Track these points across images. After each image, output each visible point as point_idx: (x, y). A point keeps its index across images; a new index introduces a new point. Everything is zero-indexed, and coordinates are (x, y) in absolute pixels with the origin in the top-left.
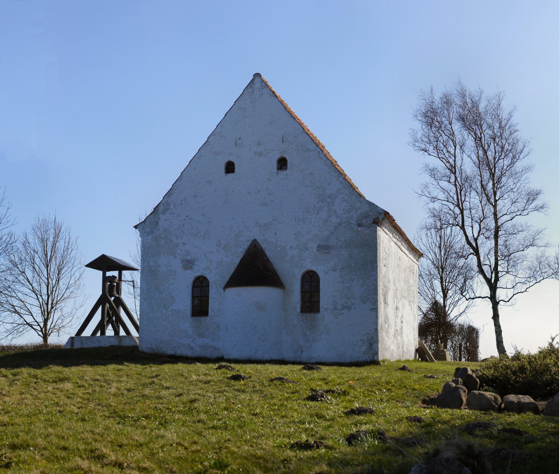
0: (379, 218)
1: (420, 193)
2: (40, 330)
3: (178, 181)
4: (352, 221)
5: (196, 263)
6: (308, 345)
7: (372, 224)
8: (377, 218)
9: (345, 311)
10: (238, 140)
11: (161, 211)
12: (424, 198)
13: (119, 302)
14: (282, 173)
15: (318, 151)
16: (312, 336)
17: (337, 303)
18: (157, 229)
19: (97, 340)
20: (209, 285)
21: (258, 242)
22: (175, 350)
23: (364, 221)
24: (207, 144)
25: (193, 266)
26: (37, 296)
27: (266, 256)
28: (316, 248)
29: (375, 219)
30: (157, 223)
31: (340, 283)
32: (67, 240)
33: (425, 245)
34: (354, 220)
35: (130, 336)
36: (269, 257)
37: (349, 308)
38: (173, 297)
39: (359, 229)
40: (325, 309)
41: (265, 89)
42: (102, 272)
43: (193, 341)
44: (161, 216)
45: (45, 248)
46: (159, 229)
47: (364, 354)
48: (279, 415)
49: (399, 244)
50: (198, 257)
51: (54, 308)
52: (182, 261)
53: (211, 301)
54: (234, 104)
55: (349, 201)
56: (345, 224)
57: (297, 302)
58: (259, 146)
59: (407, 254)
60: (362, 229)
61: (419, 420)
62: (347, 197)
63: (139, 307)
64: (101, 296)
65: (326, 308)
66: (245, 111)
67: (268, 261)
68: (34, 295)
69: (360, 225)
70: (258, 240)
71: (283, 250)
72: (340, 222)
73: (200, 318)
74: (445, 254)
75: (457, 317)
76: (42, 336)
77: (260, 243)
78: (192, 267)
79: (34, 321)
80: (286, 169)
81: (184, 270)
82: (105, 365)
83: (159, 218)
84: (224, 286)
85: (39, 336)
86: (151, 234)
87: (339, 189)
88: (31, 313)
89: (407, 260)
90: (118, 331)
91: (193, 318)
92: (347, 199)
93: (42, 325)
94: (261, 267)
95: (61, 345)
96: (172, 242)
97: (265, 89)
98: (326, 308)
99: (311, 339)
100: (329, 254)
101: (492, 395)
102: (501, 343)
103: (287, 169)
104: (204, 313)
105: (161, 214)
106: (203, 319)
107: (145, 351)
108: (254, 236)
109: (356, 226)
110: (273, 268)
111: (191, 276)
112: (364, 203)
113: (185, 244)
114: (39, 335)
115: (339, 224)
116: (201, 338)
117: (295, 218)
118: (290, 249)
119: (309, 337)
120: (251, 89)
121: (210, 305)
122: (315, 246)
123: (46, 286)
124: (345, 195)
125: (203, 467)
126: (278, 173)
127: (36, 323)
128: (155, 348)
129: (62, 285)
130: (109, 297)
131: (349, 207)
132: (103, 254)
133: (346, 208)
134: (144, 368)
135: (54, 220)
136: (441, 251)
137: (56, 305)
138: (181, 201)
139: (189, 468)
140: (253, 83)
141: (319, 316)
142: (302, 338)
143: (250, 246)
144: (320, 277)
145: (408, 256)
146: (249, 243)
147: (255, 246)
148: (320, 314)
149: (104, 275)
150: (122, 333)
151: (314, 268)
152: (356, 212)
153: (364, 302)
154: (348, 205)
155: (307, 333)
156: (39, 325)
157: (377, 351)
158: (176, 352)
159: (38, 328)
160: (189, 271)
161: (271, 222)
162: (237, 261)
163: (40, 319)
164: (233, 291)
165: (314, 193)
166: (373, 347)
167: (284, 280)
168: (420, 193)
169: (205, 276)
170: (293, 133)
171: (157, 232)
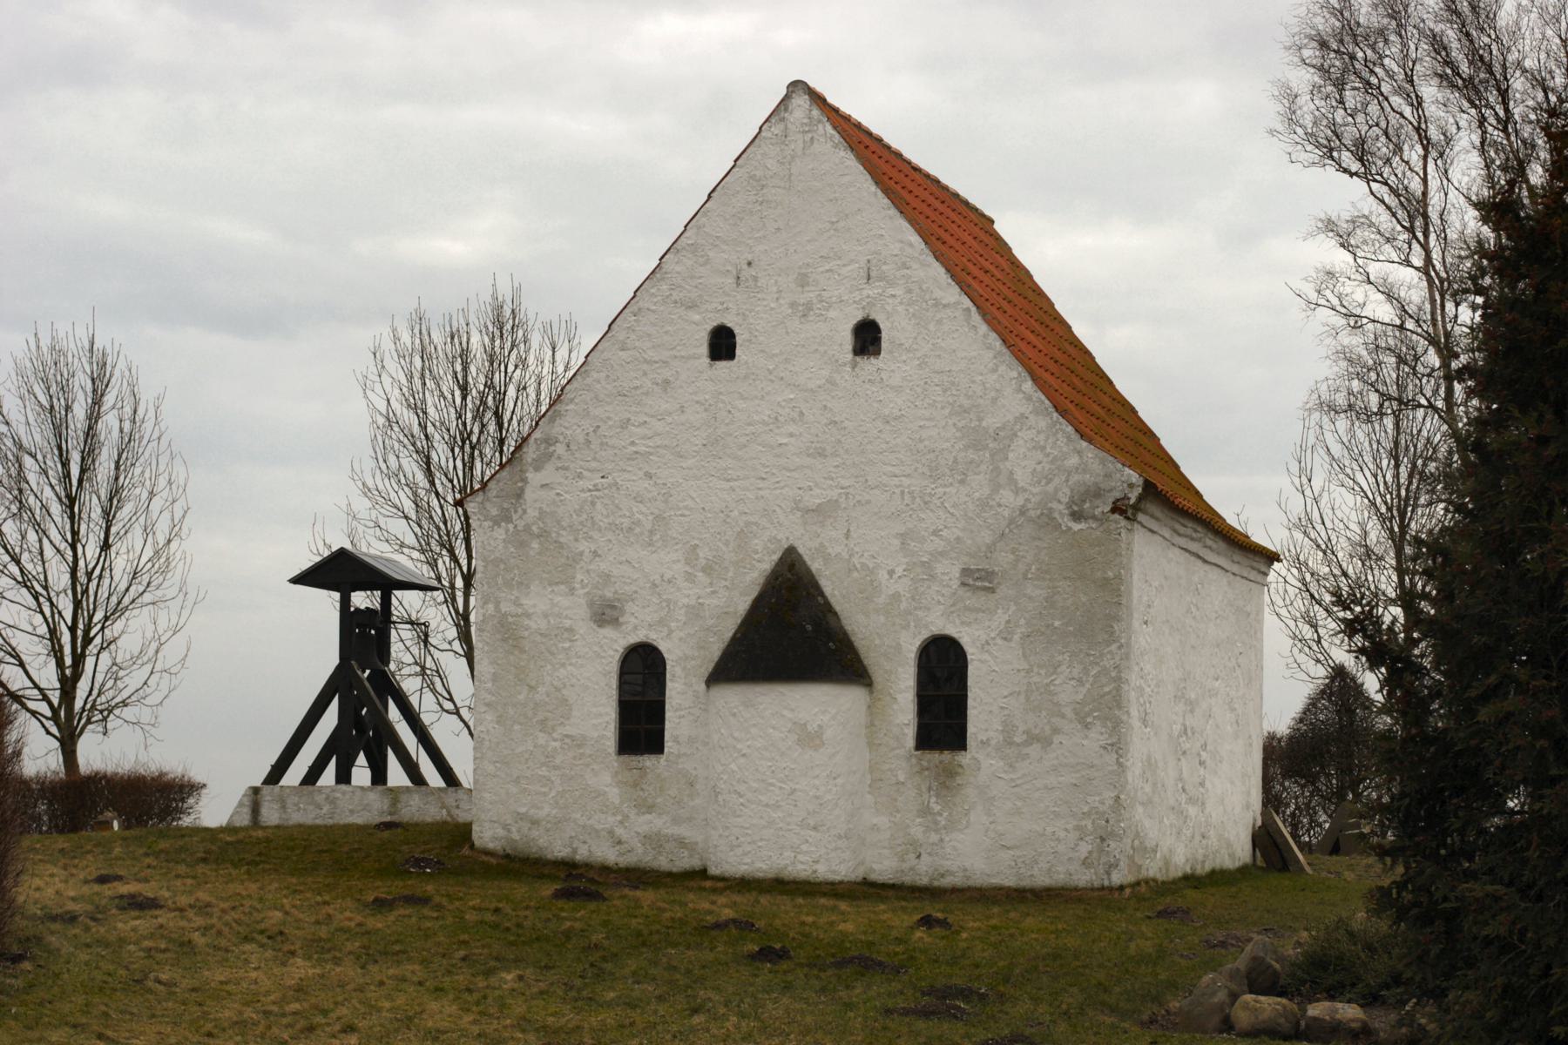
0: (1129, 499)
1: (1313, 296)
2: (49, 713)
3: (578, 377)
4: (1054, 505)
5: (629, 607)
6: (934, 837)
7: (1109, 514)
8: (1123, 499)
9: (1034, 750)
10: (745, 267)
11: (529, 460)
12: (1324, 313)
13: (387, 687)
14: (868, 365)
15: (965, 307)
16: (945, 814)
17: (1013, 726)
18: (520, 510)
19: (327, 798)
20: (665, 669)
21: (800, 555)
22: (574, 846)
23: (1087, 505)
24: (658, 275)
25: (622, 616)
26: (37, 599)
27: (822, 594)
28: (958, 575)
29: (1118, 500)
30: (519, 495)
31: (1023, 674)
32: (128, 410)
33: (1347, 444)
34: (1059, 502)
35: (423, 788)
36: (829, 598)
37: (1046, 742)
38: (567, 700)
39: (1076, 527)
40: (982, 742)
41: (820, 126)
42: (337, 595)
43: (621, 822)
44: (530, 475)
45: (59, 430)
46: (525, 512)
47: (1084, 864)
48: (846, 545)
49: (1194, 547)
50: (636, 592)
51: (98, 640)
52: (591, 604)
53: (669, 714)
54: (733, 167)
55: (1048, 450)
56: (1039, 512)
57: (906, 722)
58: (803, 286)
59: (1219, 563)
60: (1082, 526)
61: (122, 897)
62: (1042, 437)
63: (70, 656)
64: (338, 668)
65: (985, 739)
66: (763, 186)
67: (828, 608)
68: (25, 596)
69: (1077, 516)
70: (801, 550)
71: (868, 578)
72: (1023, 506)
73: (640, 758)
74: (1411, 476)
75: (1203, 867)
76: (58, 734)
77: (806, 558)
78: (617, 619)
79: (31, 685)
80: (877, 352)
81: (595, 627)
82: (389, 643)
83: (525, 480)
84: (707, 675)
85: (49, 736)
86: (503, 524)
87: (1022, 414)
88: (17, 657)
89: (119, 559)
90: (1258, 854)
91: (625, 758)
92: (1042, 443)
93: (55, 698)
94: (809, 627)
95: (144, 777)
96: (562, 548)
97: (820, 126)
98: (985, 739)
99: (943, 823)
100: (993, 592)
101: (1278, 1004)
102: (830, 617)
103: (879, 354)
104: (654, 744)
105: (531, 469)
106: (648, 761)
107: (491, 846)
108: (788, 539)
109: (1065, 520)
110: (842, 627)
111: (616, 643)
112: (1090, 455)
113: (600, 556)
114: (48, 733)
115: (1020, 510)
116: (643, 813)
117: (902, 493)
118: (887, 576)
119: (939, 818)
120: (781, 126)
121: (668, 725)
122: (956, 572)
123: (1419, 180)
124: (1039, 432)
125: (179, 828)
126: (854, 366)
127: (36, 692)
128: (518, 838)
129: (120, 563)
130: (359, 673)
131: (1047, 467)
132: (342, 548)
133: (1039, 468)
134: (1145, 722)
135: (87, 346)
136: (1397, 466)
137: (103, 628)
138: (587, 434)
139: (989, 635)
140: (786, 110)
141: (964, 758)
142: (918, 820)
143: (777, 565)
144: (969, 657)
145: (1227, 571)
146: (776, 557)
147: (792, 566)
148: (969, 756)
149: (345, 602)
150: (396, 775)
151: (951, 631)
152: (1067, 481)
153: (1087, 726)
154: (1045, 460)
155: (931, 805)
156: (45, 698)
157: (1033, 286)
158: (575, 851)
159: (43, 708)
160: (608, 632)
161: (836, 501)
162: (743, 605)
163: (48, 676)
164: (733, 696)
165: (955, 424)
166: (1108, 846)
167: (872, 658)
168: (1313, 296)
169: (655, 643)
170: (896, 256)
171: (521, 517)
